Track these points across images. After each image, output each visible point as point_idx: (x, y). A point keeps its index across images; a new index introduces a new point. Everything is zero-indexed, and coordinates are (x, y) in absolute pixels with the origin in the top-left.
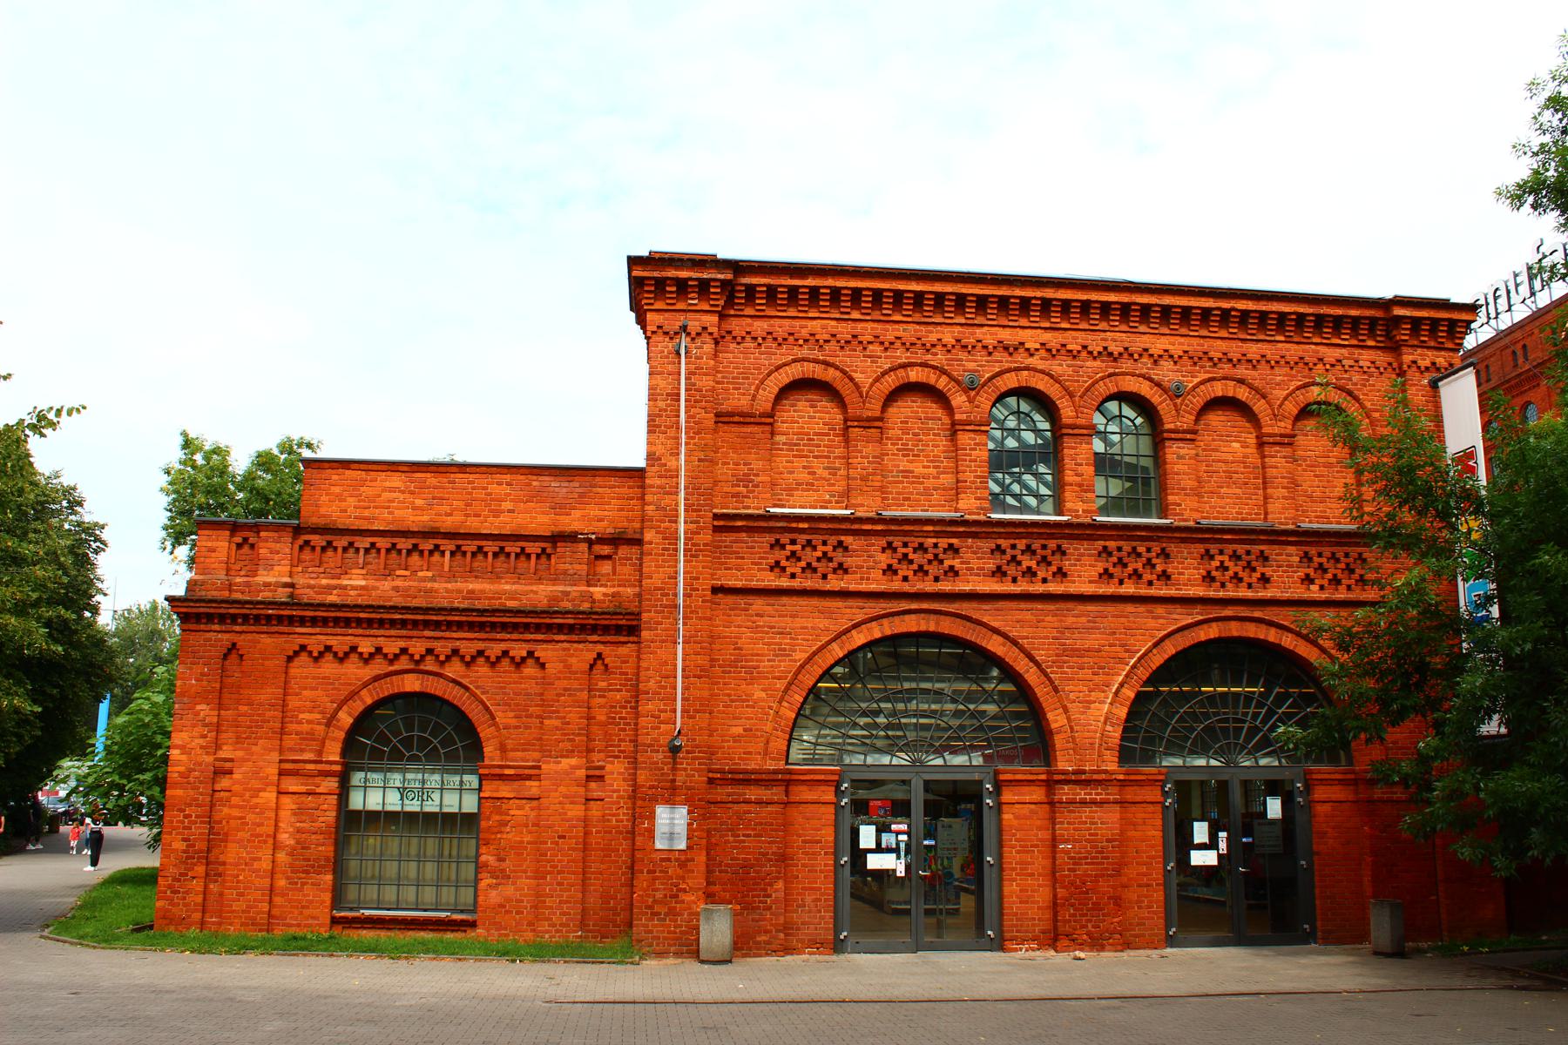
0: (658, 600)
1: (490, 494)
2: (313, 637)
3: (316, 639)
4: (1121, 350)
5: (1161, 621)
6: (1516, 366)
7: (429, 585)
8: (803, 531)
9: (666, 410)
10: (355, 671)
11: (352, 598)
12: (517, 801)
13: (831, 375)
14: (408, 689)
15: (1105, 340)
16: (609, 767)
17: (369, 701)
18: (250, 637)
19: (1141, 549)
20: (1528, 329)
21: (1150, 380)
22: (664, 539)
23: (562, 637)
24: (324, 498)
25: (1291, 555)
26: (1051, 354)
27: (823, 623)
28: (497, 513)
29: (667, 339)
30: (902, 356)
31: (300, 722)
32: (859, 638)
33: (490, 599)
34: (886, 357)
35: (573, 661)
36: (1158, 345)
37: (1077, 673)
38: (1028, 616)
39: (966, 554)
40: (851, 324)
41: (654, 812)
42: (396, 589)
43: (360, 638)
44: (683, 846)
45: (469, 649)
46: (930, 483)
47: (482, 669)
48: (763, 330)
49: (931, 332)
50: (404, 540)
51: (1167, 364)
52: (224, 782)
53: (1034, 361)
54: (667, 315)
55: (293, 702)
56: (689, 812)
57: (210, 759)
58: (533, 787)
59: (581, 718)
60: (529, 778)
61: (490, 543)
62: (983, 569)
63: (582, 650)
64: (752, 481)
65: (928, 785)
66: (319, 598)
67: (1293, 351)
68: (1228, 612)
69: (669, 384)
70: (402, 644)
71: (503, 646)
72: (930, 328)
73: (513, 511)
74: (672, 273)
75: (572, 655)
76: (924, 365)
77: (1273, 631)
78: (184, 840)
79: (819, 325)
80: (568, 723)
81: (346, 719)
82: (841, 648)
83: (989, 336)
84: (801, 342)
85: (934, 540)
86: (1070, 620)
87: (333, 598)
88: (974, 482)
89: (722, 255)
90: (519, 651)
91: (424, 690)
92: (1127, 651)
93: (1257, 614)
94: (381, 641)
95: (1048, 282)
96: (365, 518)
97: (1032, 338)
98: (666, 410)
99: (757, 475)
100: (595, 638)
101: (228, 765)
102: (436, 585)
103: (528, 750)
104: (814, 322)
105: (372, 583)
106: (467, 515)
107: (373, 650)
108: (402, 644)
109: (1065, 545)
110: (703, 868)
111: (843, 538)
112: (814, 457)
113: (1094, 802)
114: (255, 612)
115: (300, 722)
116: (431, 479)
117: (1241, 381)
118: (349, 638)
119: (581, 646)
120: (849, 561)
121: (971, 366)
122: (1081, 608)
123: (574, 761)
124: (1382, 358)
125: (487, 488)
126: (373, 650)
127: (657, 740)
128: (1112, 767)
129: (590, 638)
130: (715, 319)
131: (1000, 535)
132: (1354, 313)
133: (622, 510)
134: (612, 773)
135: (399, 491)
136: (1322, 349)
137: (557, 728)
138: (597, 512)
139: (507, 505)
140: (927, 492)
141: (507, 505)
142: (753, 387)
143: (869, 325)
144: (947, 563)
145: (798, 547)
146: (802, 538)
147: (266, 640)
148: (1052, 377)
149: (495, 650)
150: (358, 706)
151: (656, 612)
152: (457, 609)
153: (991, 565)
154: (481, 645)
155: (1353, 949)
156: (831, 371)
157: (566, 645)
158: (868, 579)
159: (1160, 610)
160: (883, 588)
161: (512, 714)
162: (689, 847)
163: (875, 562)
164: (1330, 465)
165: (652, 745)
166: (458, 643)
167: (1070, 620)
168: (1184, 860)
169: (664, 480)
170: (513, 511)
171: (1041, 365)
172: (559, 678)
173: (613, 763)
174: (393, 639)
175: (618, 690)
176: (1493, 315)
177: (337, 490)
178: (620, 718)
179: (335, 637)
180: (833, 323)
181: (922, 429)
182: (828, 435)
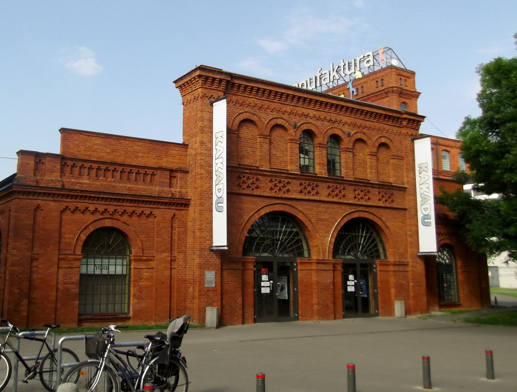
0: (205, 195)
1: (134, 150)
2: (71, 203)
3: (72, 204)
4: (335, 120)
5: (343, 211)
7: (113, 184)
8: (247, 173)
9: (207, 126)
10: (89, 218)
11: (85, 187)
12: (146, 269)
13: (255, 118)
14: (107, 225)
15: (331, 116)
16: (178, 256)
17: (92, 230)
18: (45, 202)
19: (339, 187)
21: (342, 131)
22: (207, 173)
23: (163, 207)
25: (376, 191)
26: (319, 119)
28: (137, 157)
29: (207, 99)
30: (276, 115)
31: (65, 238)
32: (263, 212)
33: (136, 191)
34: (271, 114)
35: (166, 216)
36: (345, 119)
37: (322, 227)
38: (309, 207)
40: (261, 101)
41: (204, 273)
42: (102, 185)
43: (90, 204)
44: (214, 286)
45: (130, 210)
46: (281, 159)
47: (135, 218)
48: (235, 99)
49: (284, 107)
50: (103, 165)
51: (346, 126)
52: (35, 263)
53: (311, 120)
54: (207, 90)
55: (63, 230)
56: (216, 273)
57: (29, 254)
58: (153, 264)
59: (169, 238)
60: (150, 260)
61: (134, 169)
62: (297, 190)
63: (169, 212)
64: (231, 154)
65: (278, 263)
66: (72, 187)
67: (378, 125)
68: (361, 209)
69: (208, 116)
70: (106, 207)
71: (142, 209)
72: (284, 105)
73: (142, 157)
74: (211, 75)
75: (165, 214)
76: (282, 118)
77: (371, 215)
78: (18, 289)
79: (252, 100)
80: (164, 240)
81: (83, 237)
82: (258, 215)
83: (300, 110)
84: (246, 105)
85: (284, 179)
86: (320, 209)
87: (77, 187)
88: (295, 160)
89: (225, 69)
90: (147, 211)
91: (113, 226)
92: (335, 220)
93: (367, 210)
95: (238, 77)
96: (89, 155)
97: (312, 113)
98: (207, 126)
99: (233, 152)
100: (174, 208)
101: (36, 256)
102: (116, 185)
103: (150, 250)
104: (251, 99)
105: (92, 182)
106: (126, 157)
107: (94, 209)
108: (106, 207)
109: (319, 183)
111: (258, 177)
112: (249, 147)
113: (326, 270)
114: (98, 196)
115: (65, 238)
116: (112, 142)
117: (364, 134)
118: (86, 204)
119: (168, 210)
120: (261, 185)
121: (295, 120)
122: (323, 205)
123: (166, 254)
125: (133, 147)
126: (94, 209)
127: (205, 247)
129: (172, 208)
131: (303, 179)
132: (394, 115)
133: (180, 160)
134: (179, 259)
135: (101, 145)
136: (385, 125)
137: (161, 242)
138: (172, 160)
139: (140, 154)
141: (140, 154)
142: (232, 120)
143: (267, 102)
144: (287, 188)
145: (245, 179)
146: (247, 175)
147: (52, 204)
148: (316, 126)
149: (139, 211)
150: (88, 232)
151: (205, 200)
152: (88, 191)
153: (299, 189)
154: (134, 209)
156: (255, 117)
157: (164, 210)
158: (266, 191)
159: (343, 207)
160: (267, 194)
161: (144, 236)
162: (216, 286)
163: (268, 186)
164: (384, 163)
165: (204, 249)
166: (126, 208)
167: (320, 209)
168: (346, 289)
169: (206, 151)
170: (142, 157)
171: (314, 122)
172: (161, 223)
173: (179, 255)
174: (102, 205)
175: (181, 228)
176: (332, 80)
177: (77, 142)
178: (182, 238)
179: (80, 204)
180: (256, 100)
181: (279, 140)
182: (252, 139)
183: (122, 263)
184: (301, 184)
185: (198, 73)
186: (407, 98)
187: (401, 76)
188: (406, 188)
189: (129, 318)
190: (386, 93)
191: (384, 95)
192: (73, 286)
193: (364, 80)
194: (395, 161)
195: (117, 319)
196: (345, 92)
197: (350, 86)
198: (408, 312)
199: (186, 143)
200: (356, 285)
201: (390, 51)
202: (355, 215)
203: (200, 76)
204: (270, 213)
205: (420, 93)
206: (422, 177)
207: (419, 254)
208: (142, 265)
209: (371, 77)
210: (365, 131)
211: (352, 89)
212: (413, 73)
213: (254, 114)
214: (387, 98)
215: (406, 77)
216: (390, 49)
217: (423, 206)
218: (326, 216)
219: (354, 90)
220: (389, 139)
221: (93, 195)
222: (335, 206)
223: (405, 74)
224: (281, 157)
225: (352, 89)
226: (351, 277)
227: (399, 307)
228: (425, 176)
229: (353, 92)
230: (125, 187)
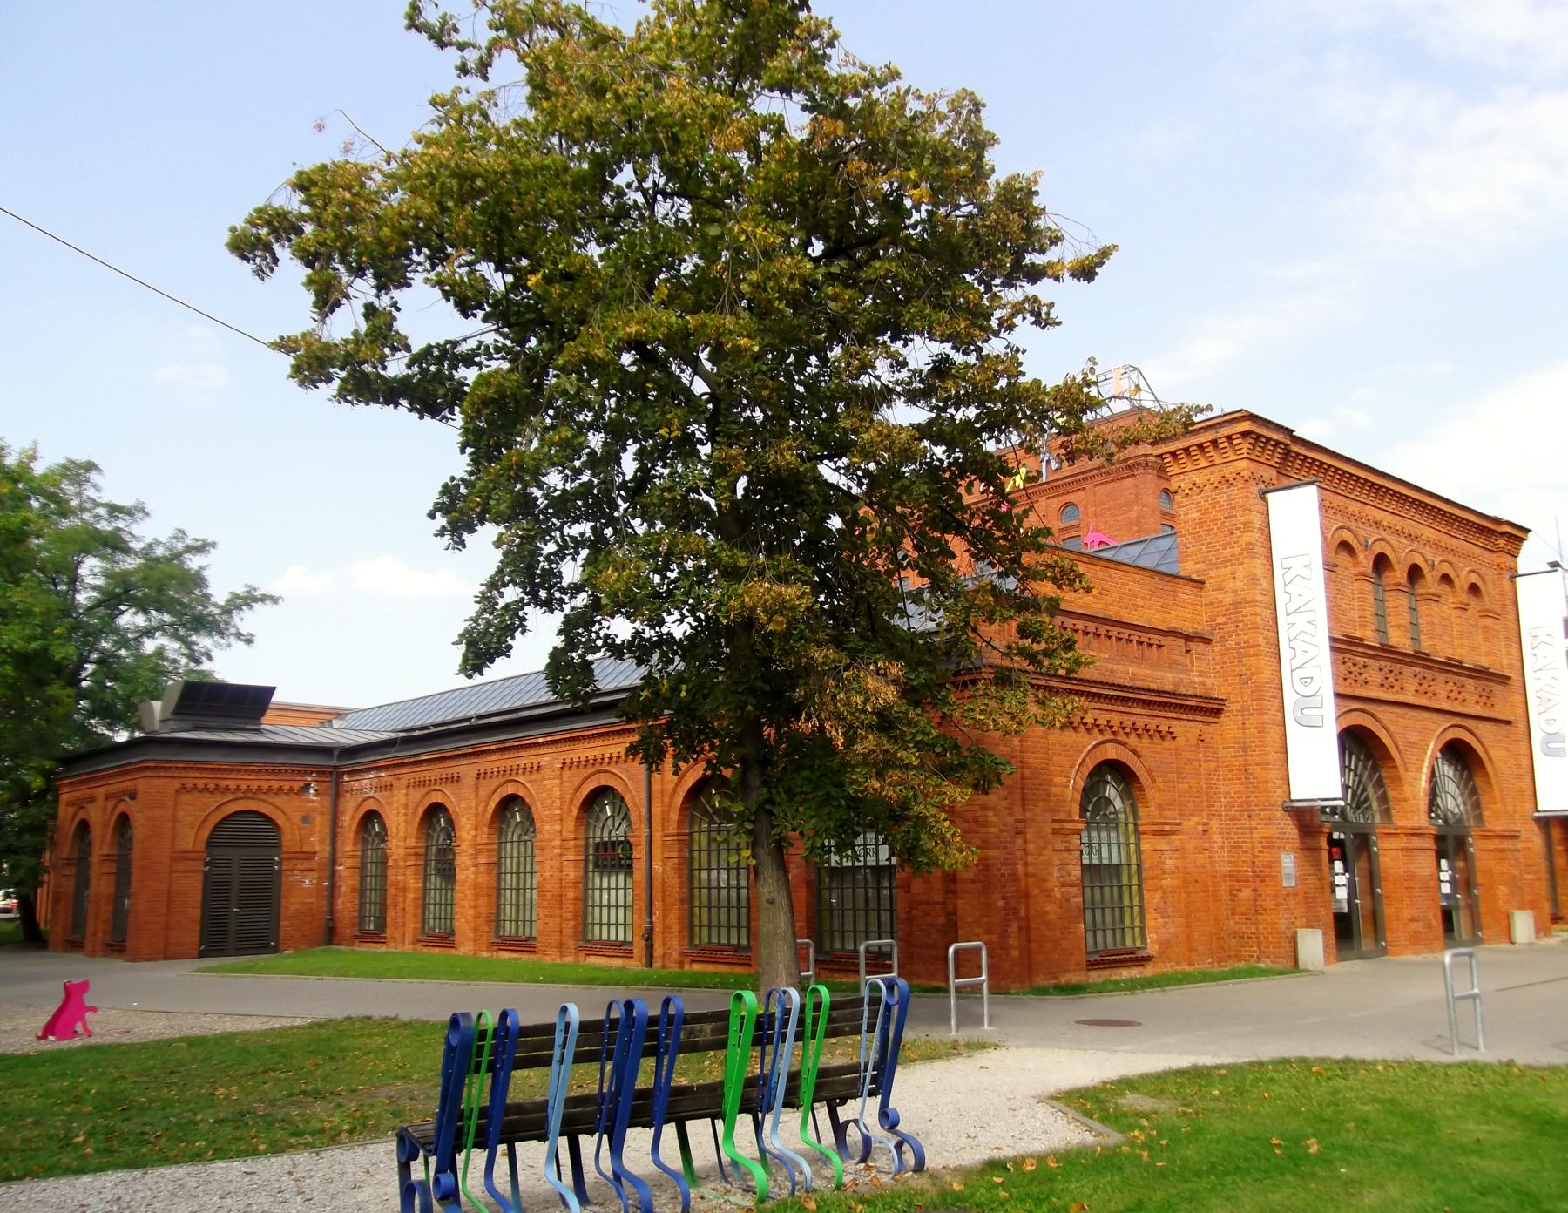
35: (1189, 735)
60: (1172, 832)
183: (877, 840)
185: (1245, 426)
188: (1508, 678)
189: (1149, 959)
190: (1129, 467)
191: (1126, 473)
192: (1074, 890)
194: (1488, 622)
195: (1132, 960)
198: (1541, 930)
201: (1136, 373)
203: (1245, 434)
206: (1299, 652)
207: (1537, 814)
208: (1162, 843)
214: (1131, 480)
216: (1136, 369)
217: (1545, 716)
221: (1094, 690)
222: (1426, 715)
226: (1444, 863)
227: (1523, 924)
228: (1306, 647)
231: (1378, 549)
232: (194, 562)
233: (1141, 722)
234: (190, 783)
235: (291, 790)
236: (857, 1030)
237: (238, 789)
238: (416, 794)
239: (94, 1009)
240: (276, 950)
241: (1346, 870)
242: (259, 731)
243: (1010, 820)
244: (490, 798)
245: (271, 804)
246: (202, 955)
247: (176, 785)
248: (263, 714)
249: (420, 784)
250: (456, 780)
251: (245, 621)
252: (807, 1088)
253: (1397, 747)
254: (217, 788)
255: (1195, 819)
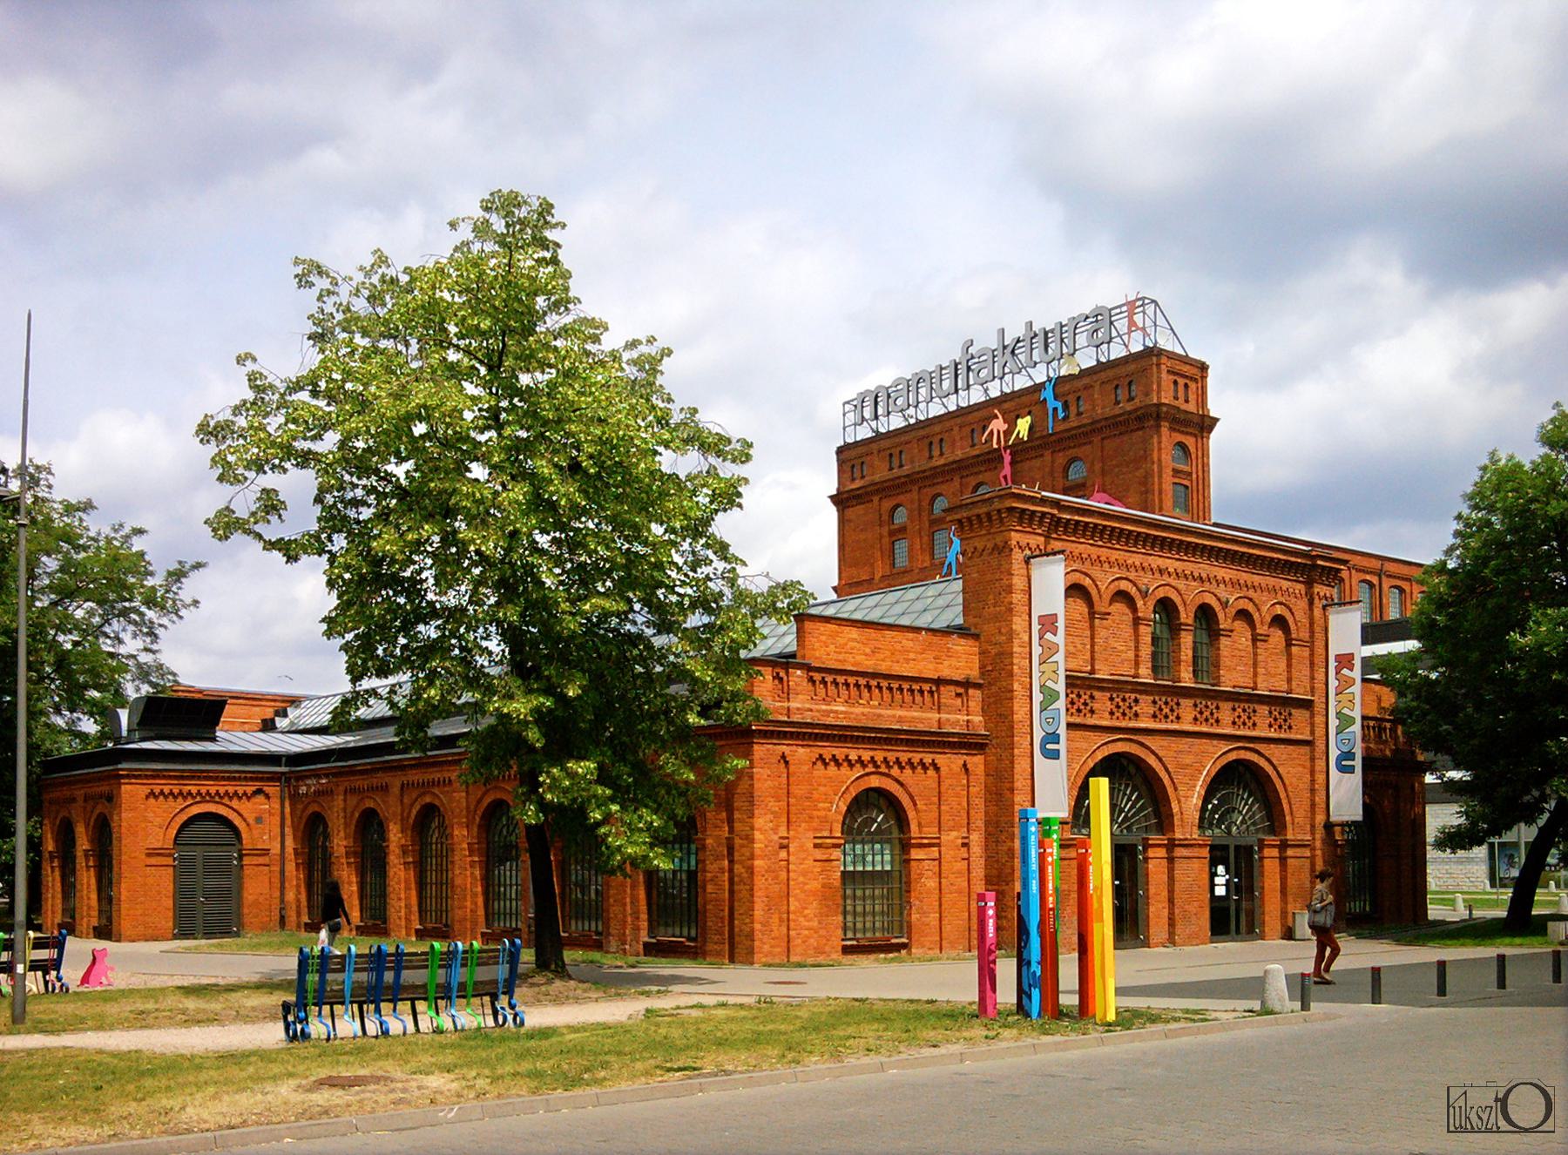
6: (931, 457)
14: (873, 785)
20: (947, 424)
24: (817, 645)
27: (1085, 745)
35: (953, 766)
38: (1165, 743)
39: (1142, 704)
76: (1126, 579)
83: (1156, 562)
93: (1251, 745)
94: (861, 752)
97: (1172, 565)
102: (883, 712)
110: (757, 894)
121: (1146, 581)
124: (1300, 588)
128: (1195, 836)
130: (1042, 539)
139: (912, 656)
140: (1122, 662)
147: (801, 750)
155: (221, 945)
171: (1174, 583)
177: (823, 638)
184: (1154, 702)
186: (1187, 433)
187: (1177, 374)
193: (1086, 381)
196: (1033, 408)
197: (1048, 394)
199: (1346, 750)
200: (1227, 884)
202: (1233, 756)
204: (1110, 756)
205: (1216, 420)
209: (1103, 375)
210: (1251, 593)
211: (1052, 404)
212: (1203, 367)
213: (1086, 574)
214: (1140, 433)
215: (1187, 377)
218: (1188, 760)
219: (1059, 405)
220: (1288, 607)
223: (1185, 369)
224: (1121, 651)
225: (1052, 404)
226: (1221, 869)
229: (1055, 409)
230: (894, 716)
231: (1161, 593)
232: (138, 544)
233: (904, 757)
234: (157, 791)
235: (245, 794)
236: (497, 963)
237: (199, 793)
238: (353, 800)
239: (112, 969)
240: (237, 935)
241: (1227, 873)
242: (213, 739)
243: (776, 838)
244: (412, 805)
245: (227, 806)
246: (175, 937)
247: (147, 790)
248: (217, 724)
249: (353, 791)
250: (385, 789)
251: (188, 589)
252: (470, 991)
253: (1167, 770)
254: (181, 793)
255: (954, 834)
